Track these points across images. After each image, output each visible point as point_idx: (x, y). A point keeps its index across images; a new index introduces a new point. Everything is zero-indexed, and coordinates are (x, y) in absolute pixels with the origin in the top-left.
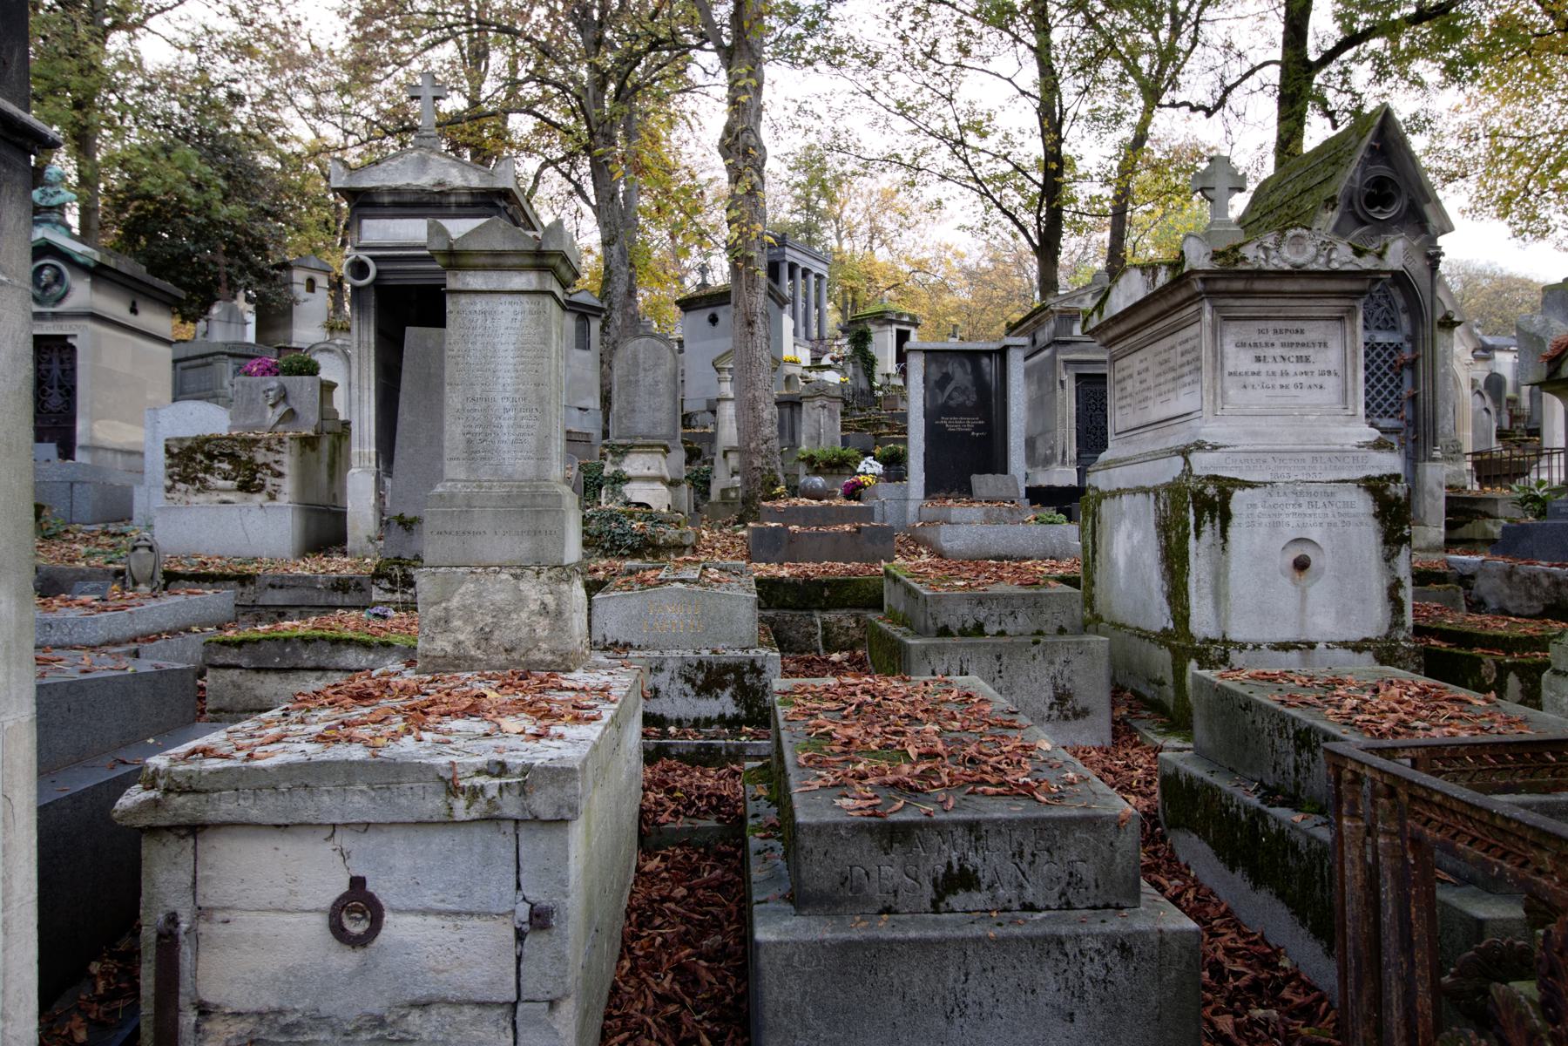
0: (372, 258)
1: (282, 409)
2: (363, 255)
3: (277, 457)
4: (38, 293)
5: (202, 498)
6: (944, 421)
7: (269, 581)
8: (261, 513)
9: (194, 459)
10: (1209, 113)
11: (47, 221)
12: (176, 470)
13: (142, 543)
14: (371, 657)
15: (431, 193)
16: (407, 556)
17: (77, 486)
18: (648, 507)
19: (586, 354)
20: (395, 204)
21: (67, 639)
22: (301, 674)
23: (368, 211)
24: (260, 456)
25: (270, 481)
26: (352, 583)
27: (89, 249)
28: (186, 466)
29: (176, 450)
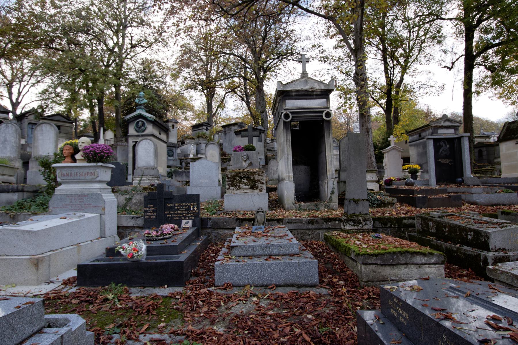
0: (290, 112)
1: (248, 162)
2: (288, 112)
3: (262, 178)
4: (137, 129)
5: (238, 191)
6: (440, 160)
7: (287, 221)
8: (258, 196)
9: (236, 179)
10: (450, 69)
11: (140, 108)
12: (230, 182)
13: (260, 210)
14: (426, 259)
15: (309, 91)
16: (357, 213)
17: (170, 187)
18: (373, 190)
19: (261, 143)
20: (296, 95)
21: (287, 252)
22: (399, 266)
23: (288, 98)
24: (257, 177)
25: (260, 185)
26: (315, 221)
27: (152, 116)
28: (233, 181)
29: (230, 176)
